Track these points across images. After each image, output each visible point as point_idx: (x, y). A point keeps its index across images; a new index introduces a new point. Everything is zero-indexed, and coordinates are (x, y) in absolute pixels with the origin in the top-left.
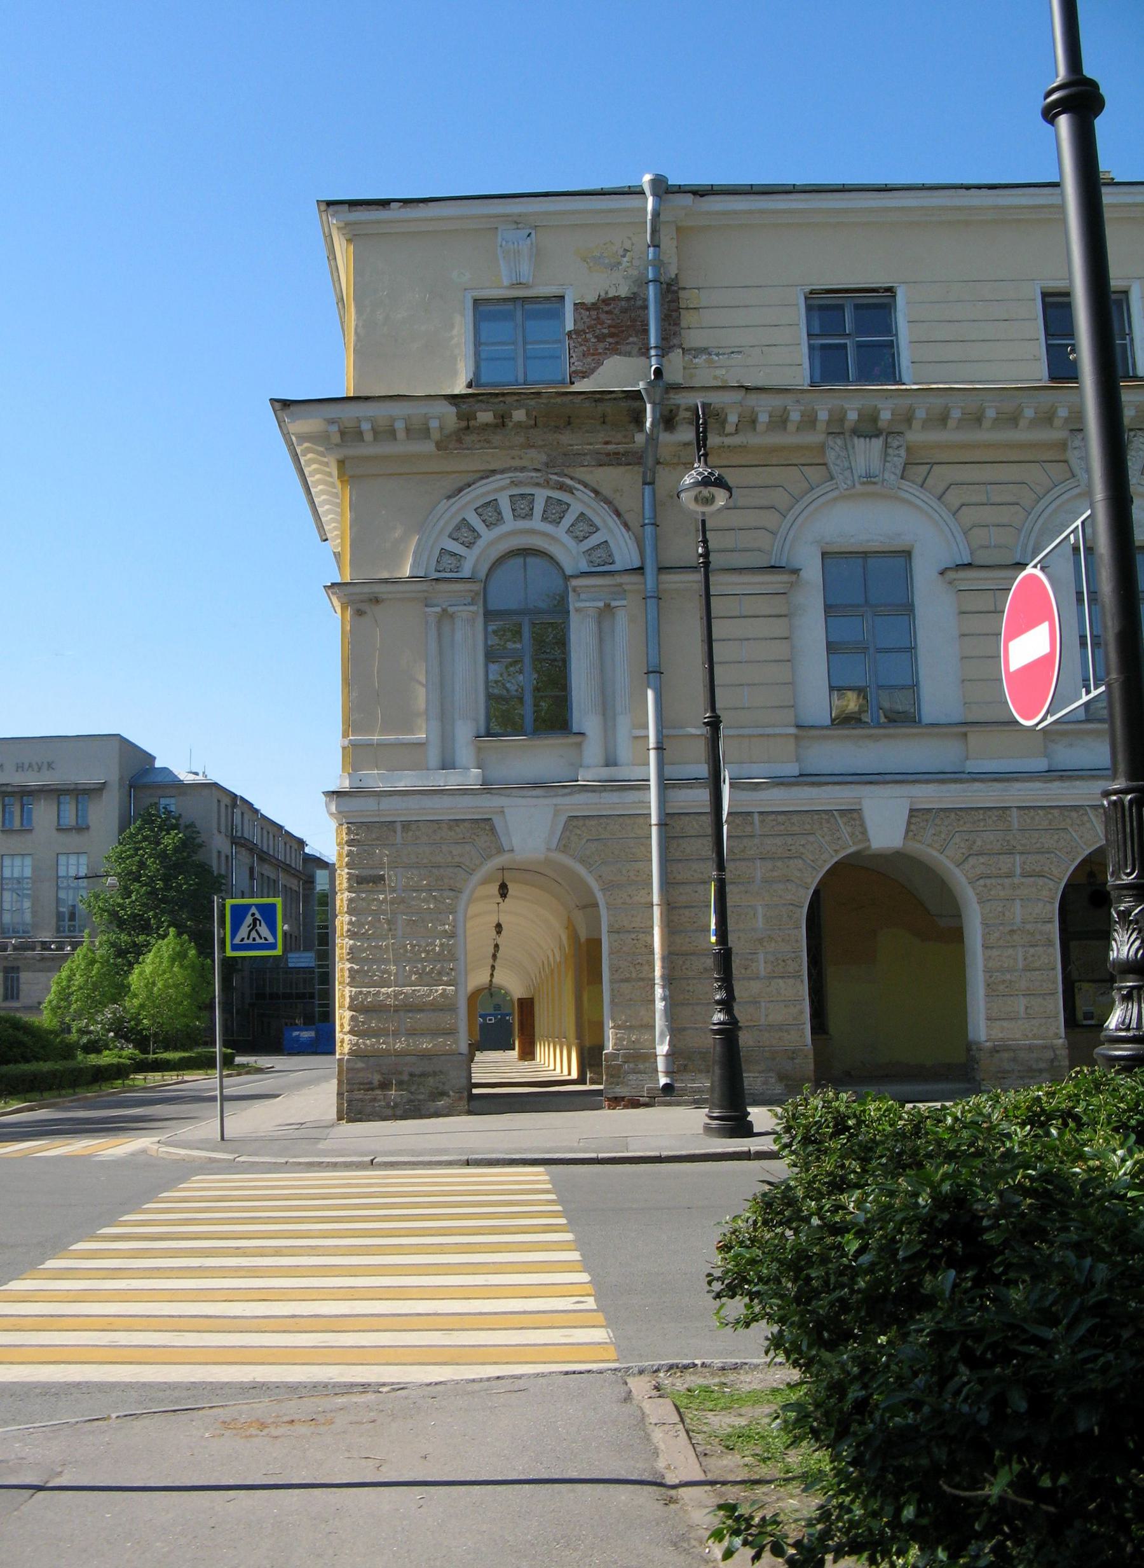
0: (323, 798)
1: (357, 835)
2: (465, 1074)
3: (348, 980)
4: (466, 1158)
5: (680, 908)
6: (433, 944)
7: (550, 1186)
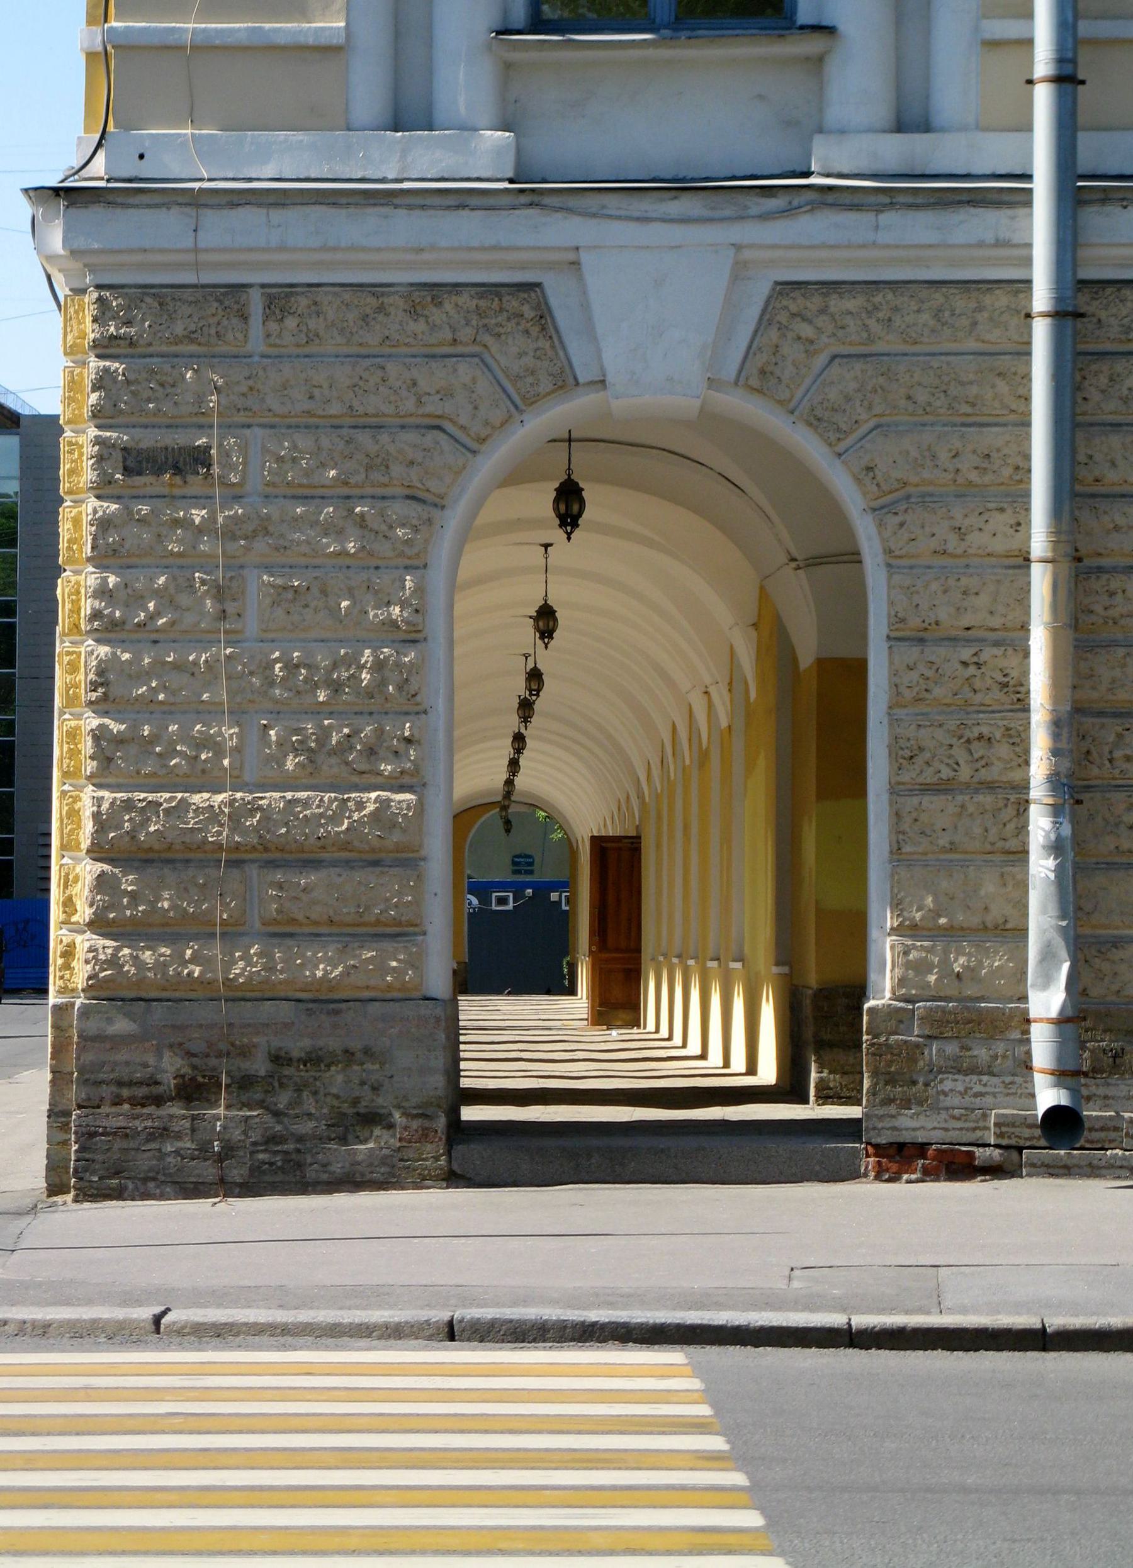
0: (25, 209)
1: (128, 323)
2: (439, 1061)
3: (90, 766)
4: (445, 1316)
5: (1114, 570)
6: (352, 661)
7: (705, 1410)
